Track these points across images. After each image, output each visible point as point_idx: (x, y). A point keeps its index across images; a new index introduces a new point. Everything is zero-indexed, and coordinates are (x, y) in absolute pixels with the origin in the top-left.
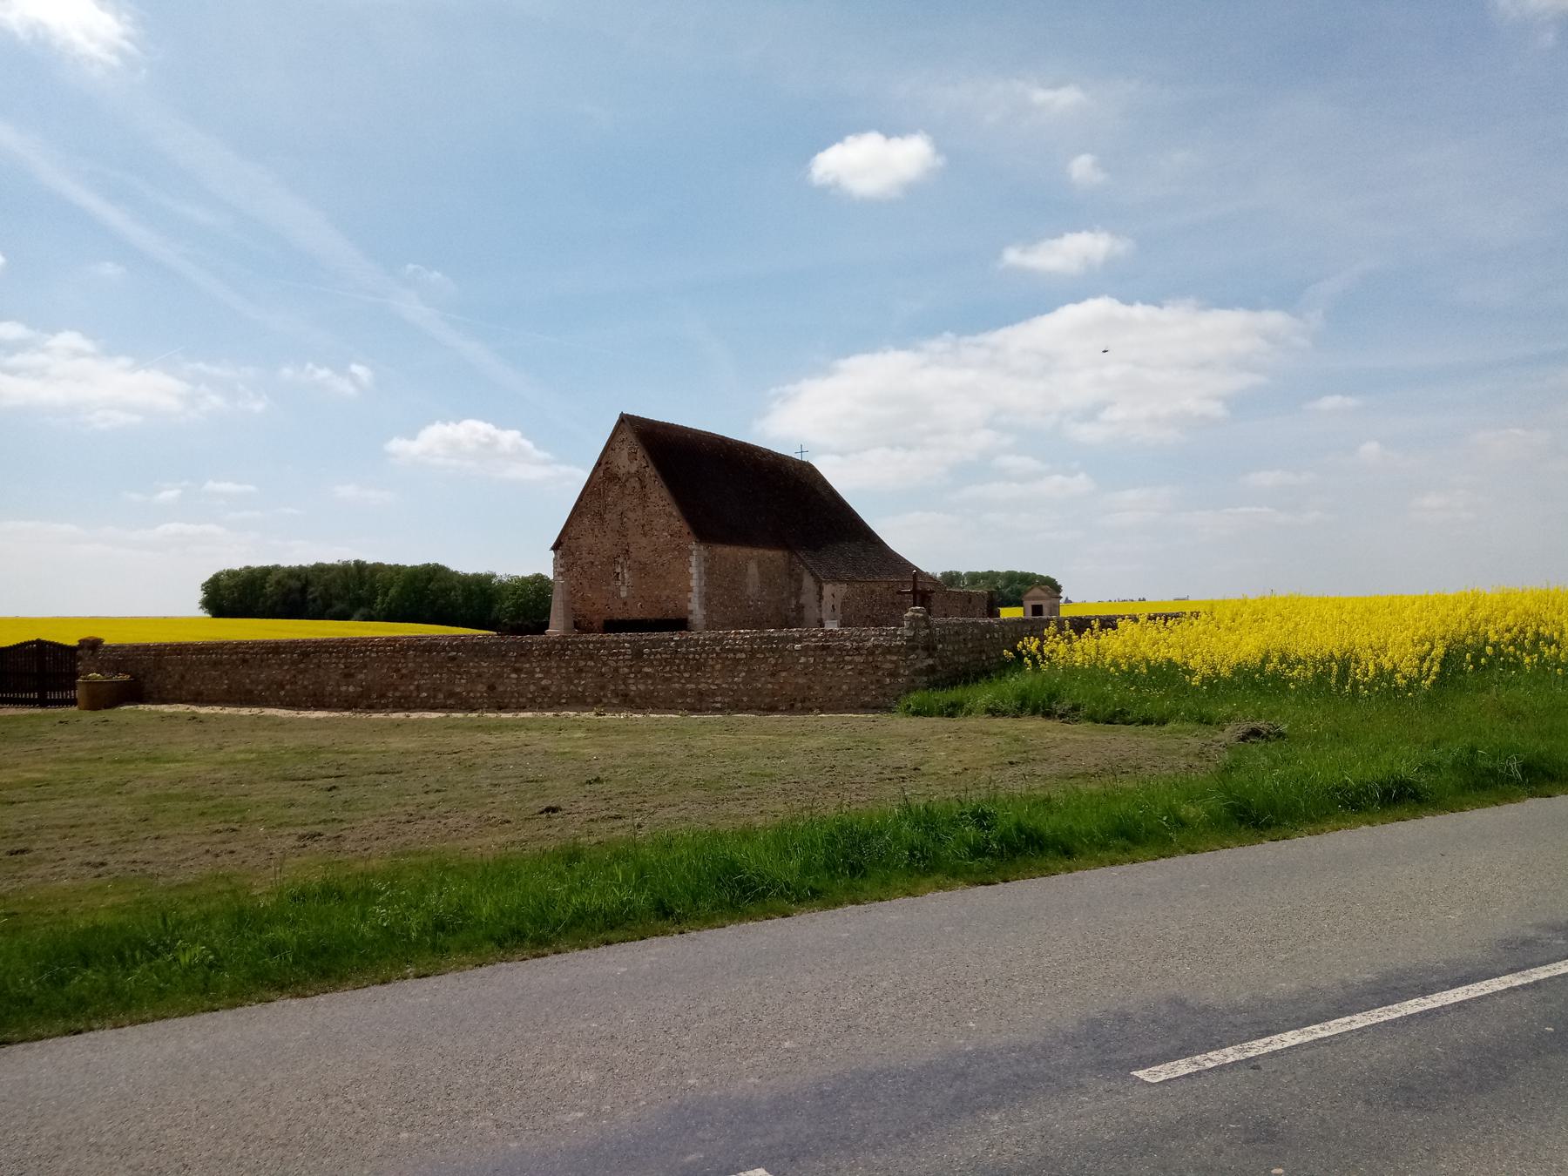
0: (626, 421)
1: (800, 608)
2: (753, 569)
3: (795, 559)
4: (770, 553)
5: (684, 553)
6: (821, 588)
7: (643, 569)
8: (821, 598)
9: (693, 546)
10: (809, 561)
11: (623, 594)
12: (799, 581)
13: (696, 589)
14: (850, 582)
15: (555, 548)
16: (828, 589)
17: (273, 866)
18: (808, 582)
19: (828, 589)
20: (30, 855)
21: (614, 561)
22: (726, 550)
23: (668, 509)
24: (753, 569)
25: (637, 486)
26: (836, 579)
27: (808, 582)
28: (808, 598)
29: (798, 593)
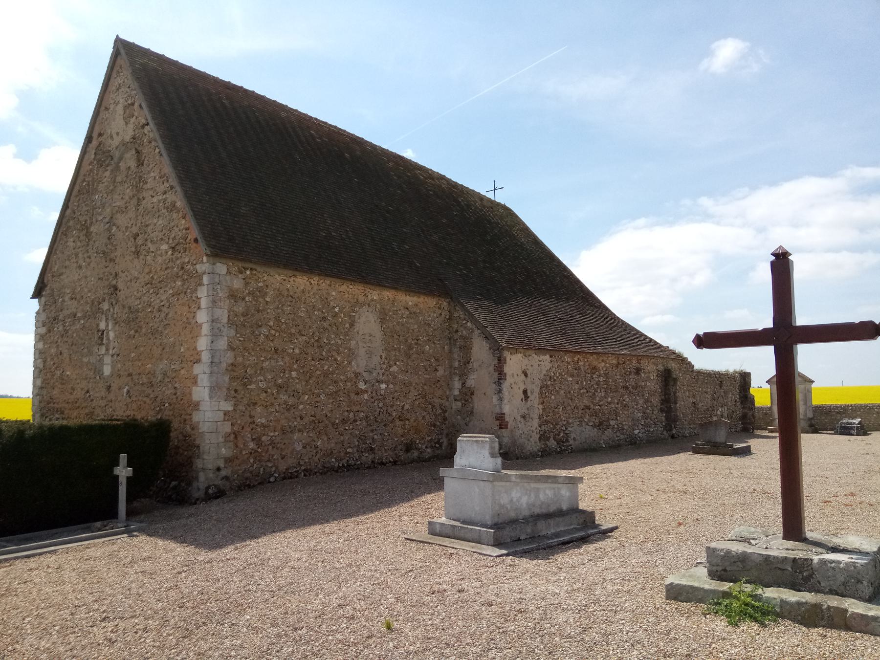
0: (749, 374)
1: (468, 394)
2: (368, 324)
3: (459, 314)
4: (410, 300)
5: (193, 279)
6: (501, 361)
7: (132, 321)
8: (501, 377)
9: (204, 266)
10: (482, 316)
11: (107, 370)
12: (466, 349)
13: (205, 357)
14: (554, 351)
15: (38, 293)
16: (514, 363)
17: (552, 522)
18: (480, 350)
19: (514, 363)
20: (406, 536)
21: (96, 311)
22: (276, 279)
23: (170, 197)
24: (368, 324)
25: (133, 164)
26: (529, 346)
27: (480, 350)
28: (480, 378)
29: (465, 368)
